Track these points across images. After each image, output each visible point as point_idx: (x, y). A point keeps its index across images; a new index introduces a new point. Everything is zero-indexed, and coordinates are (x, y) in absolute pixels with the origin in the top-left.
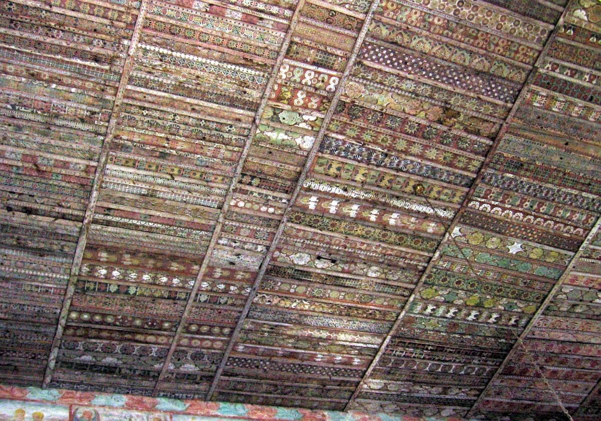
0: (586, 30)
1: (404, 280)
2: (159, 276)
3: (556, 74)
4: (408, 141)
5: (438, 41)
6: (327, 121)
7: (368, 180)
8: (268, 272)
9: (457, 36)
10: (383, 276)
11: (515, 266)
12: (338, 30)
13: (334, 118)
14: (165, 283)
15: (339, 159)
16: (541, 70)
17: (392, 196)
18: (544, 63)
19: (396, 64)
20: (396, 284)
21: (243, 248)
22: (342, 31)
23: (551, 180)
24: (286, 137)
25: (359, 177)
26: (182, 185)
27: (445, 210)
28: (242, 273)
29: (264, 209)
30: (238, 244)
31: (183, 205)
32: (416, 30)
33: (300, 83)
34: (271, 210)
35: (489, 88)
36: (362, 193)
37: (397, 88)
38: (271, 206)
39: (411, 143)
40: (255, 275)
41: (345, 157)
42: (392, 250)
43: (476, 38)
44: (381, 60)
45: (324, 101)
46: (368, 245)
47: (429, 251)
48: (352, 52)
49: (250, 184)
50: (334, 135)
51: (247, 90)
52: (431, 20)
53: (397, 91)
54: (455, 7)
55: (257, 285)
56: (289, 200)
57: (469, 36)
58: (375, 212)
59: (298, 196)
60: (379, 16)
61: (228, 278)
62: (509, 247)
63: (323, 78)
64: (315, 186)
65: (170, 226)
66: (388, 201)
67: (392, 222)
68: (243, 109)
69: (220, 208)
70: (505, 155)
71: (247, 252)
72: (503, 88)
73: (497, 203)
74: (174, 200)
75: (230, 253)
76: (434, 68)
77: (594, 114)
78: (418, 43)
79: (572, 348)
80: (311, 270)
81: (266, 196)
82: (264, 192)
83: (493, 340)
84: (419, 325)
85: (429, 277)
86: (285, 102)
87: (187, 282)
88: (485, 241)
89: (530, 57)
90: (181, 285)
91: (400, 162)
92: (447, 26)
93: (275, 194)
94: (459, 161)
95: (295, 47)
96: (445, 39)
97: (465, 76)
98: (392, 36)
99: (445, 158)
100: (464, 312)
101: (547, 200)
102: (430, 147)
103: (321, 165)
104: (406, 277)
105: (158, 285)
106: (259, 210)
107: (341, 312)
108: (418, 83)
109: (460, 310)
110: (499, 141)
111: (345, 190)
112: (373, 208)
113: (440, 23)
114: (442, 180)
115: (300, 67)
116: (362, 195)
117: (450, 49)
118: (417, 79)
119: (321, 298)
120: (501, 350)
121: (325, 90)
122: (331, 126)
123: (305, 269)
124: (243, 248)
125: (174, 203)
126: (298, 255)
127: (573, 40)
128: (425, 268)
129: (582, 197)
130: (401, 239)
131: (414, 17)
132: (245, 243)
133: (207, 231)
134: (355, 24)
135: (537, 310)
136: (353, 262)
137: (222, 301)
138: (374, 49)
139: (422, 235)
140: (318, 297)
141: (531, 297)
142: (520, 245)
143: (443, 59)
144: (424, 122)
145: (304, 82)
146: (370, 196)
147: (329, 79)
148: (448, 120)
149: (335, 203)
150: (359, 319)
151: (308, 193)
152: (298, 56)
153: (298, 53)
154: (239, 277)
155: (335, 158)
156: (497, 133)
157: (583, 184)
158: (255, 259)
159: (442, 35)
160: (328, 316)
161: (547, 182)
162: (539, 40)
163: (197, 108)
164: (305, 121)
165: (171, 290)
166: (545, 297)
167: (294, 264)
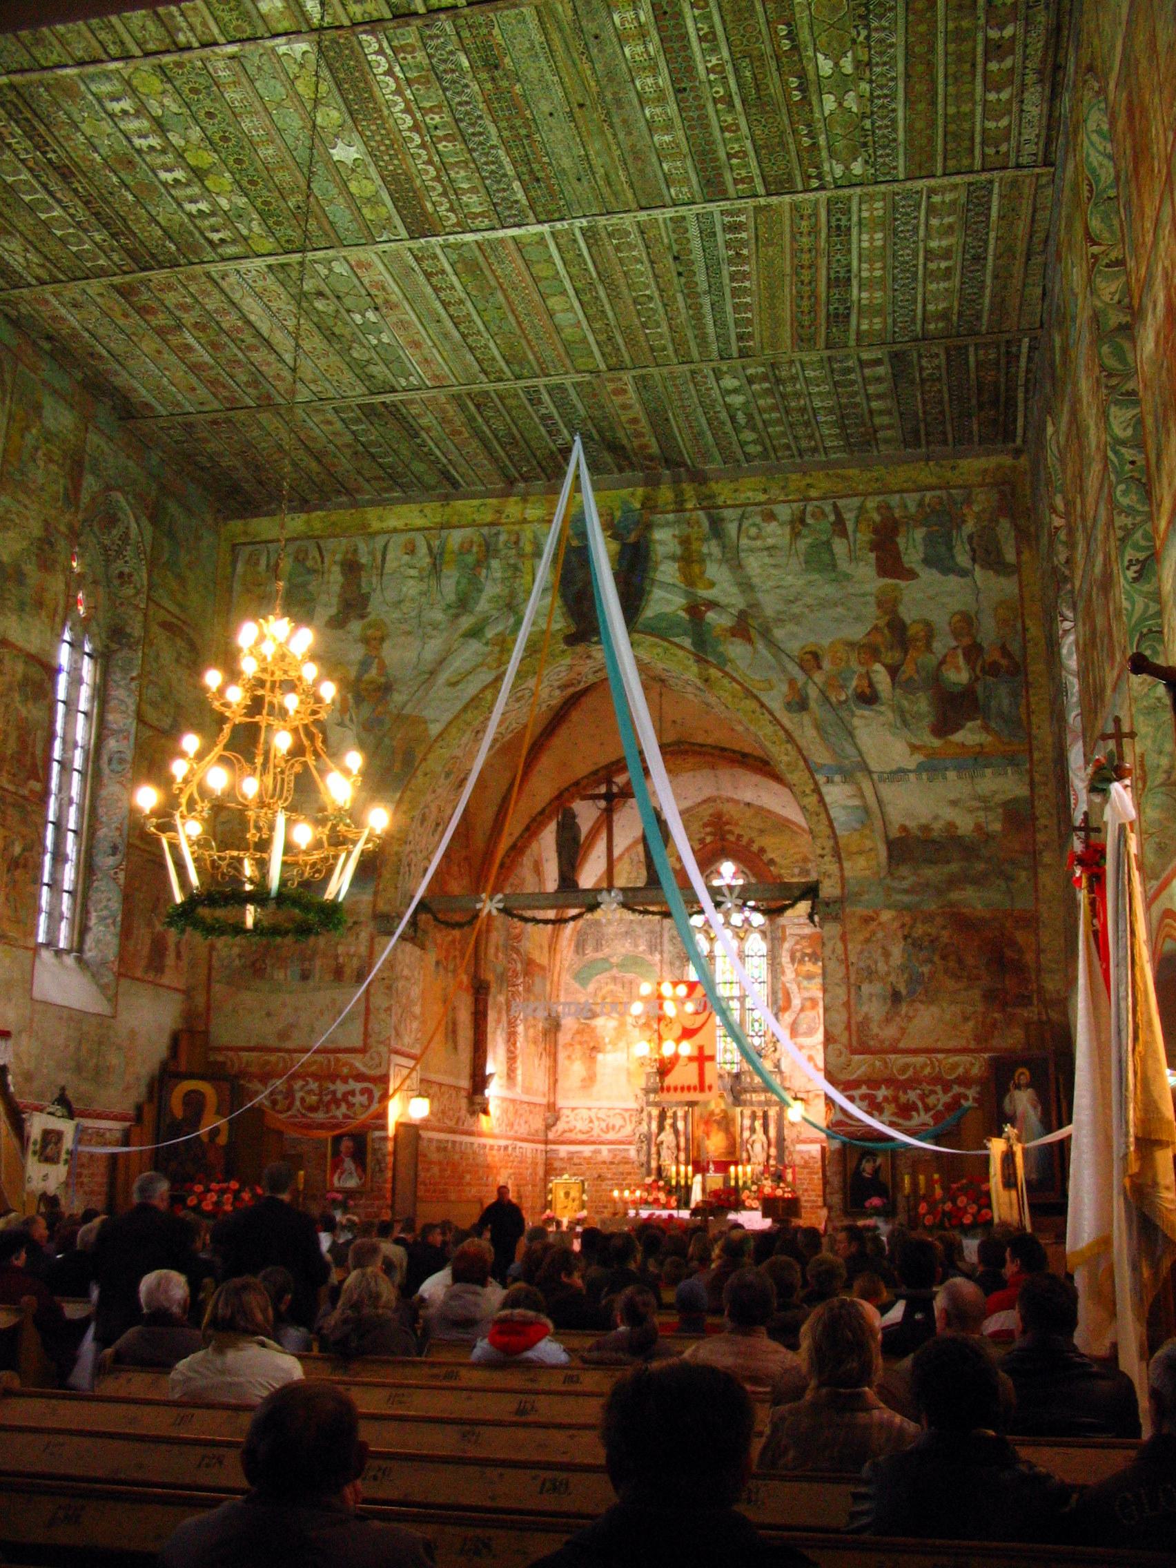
23: (504, 124)
62: (340, 144)
70: (496, 31)
77: (658, 110)
104: (143, 27)
135: (270, 254)
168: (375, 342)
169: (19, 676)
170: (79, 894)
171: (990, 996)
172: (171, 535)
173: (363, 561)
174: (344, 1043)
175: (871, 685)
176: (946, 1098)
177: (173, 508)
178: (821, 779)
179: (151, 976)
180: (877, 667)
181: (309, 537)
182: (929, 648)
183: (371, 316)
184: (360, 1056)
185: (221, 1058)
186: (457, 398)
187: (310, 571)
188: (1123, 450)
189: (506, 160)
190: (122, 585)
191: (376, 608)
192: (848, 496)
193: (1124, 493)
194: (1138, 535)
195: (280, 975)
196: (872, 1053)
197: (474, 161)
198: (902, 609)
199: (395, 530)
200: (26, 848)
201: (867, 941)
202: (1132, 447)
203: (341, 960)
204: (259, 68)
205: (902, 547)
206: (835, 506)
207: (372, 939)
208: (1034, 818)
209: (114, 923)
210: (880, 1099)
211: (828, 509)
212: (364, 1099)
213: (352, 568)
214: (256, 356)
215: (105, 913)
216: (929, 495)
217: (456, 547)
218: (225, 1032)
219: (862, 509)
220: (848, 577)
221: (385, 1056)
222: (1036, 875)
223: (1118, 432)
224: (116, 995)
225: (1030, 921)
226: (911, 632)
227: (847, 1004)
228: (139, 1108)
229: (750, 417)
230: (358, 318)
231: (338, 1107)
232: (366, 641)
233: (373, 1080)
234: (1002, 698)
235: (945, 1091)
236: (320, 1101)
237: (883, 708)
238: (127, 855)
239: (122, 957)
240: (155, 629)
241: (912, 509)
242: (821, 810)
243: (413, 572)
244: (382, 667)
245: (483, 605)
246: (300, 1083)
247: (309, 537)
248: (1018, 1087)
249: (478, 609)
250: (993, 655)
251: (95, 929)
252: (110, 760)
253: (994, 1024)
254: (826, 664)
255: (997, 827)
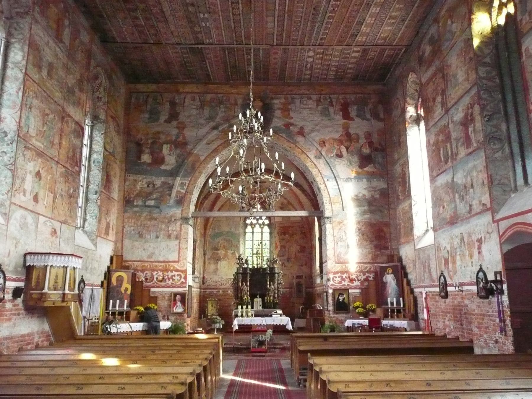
79: (160, 18)
168: (204, 25)
169: (73, 128)
170: (83, 208)
171: (376, 247)
172: (113, 86)
173: (177, 101)
174: (171, 259)
175: (340, 152)
176: (364, 277)
177: (114, 77)
178: (325, 180)
179: (105, 237)
180: (342, 146)
181: (159, 92)
182: (358, 141)
183: (206, 15)
184: (177, 263)
185: (127, 265)
186: (224, 50)
187: (158, 103)
188: (483, 81)
190: (98, 101)
191: (182, 117)
192: (334, 94)
193: (484, 94)
194: (488, 107)
195: (148, 237)
196: (342, 263)
198: (350, 130)
199: (187, 93)
200: (74, 191)
201: (340, 229)
202: (486, 80)
203: (170, 232)
205: (350, 111)
206: (330, 97)
207: (181, 225)
208: (389, 194)
209: (96, 218)
210: (344, 277)
211: (328, 98)
212: (178, 278)
213: (173, 104)
214: (161, 25)
215: (93, 214)
216: (358, 95)
217: (209, 99)
218: (128, 256)
219: (338, 98)
220: (334, 119)
221: (186, 263)
222: (389, 210)
223: (481, 75)
224: (96, 243)
225: (387, 225)
226: (353, 136)
227: (334, 248)
228: (102, 283)
229: (312, 66)
230: (202, 16)
231: (169, 280)
232: (178, 128)
233: (182, 271)
234: (379, 158)
235: (364, 275)
236: (163, 278)
237: (344, 159)
238: (100, 195)
239: (98, 229)
240: (109, 118)
241: (353, 99)
242: (326, 189)
243: (194, 107)
244: (184, 137)
245: (218, 119)
246: (156, 273)
247: (159, 92)
248: (388, 274)
249: (216, 120)
250: (376, 145)
251: (88, 220)
252: (94, 161)
253: (378, 255)
254: (327, 145)
255: (377, 196)
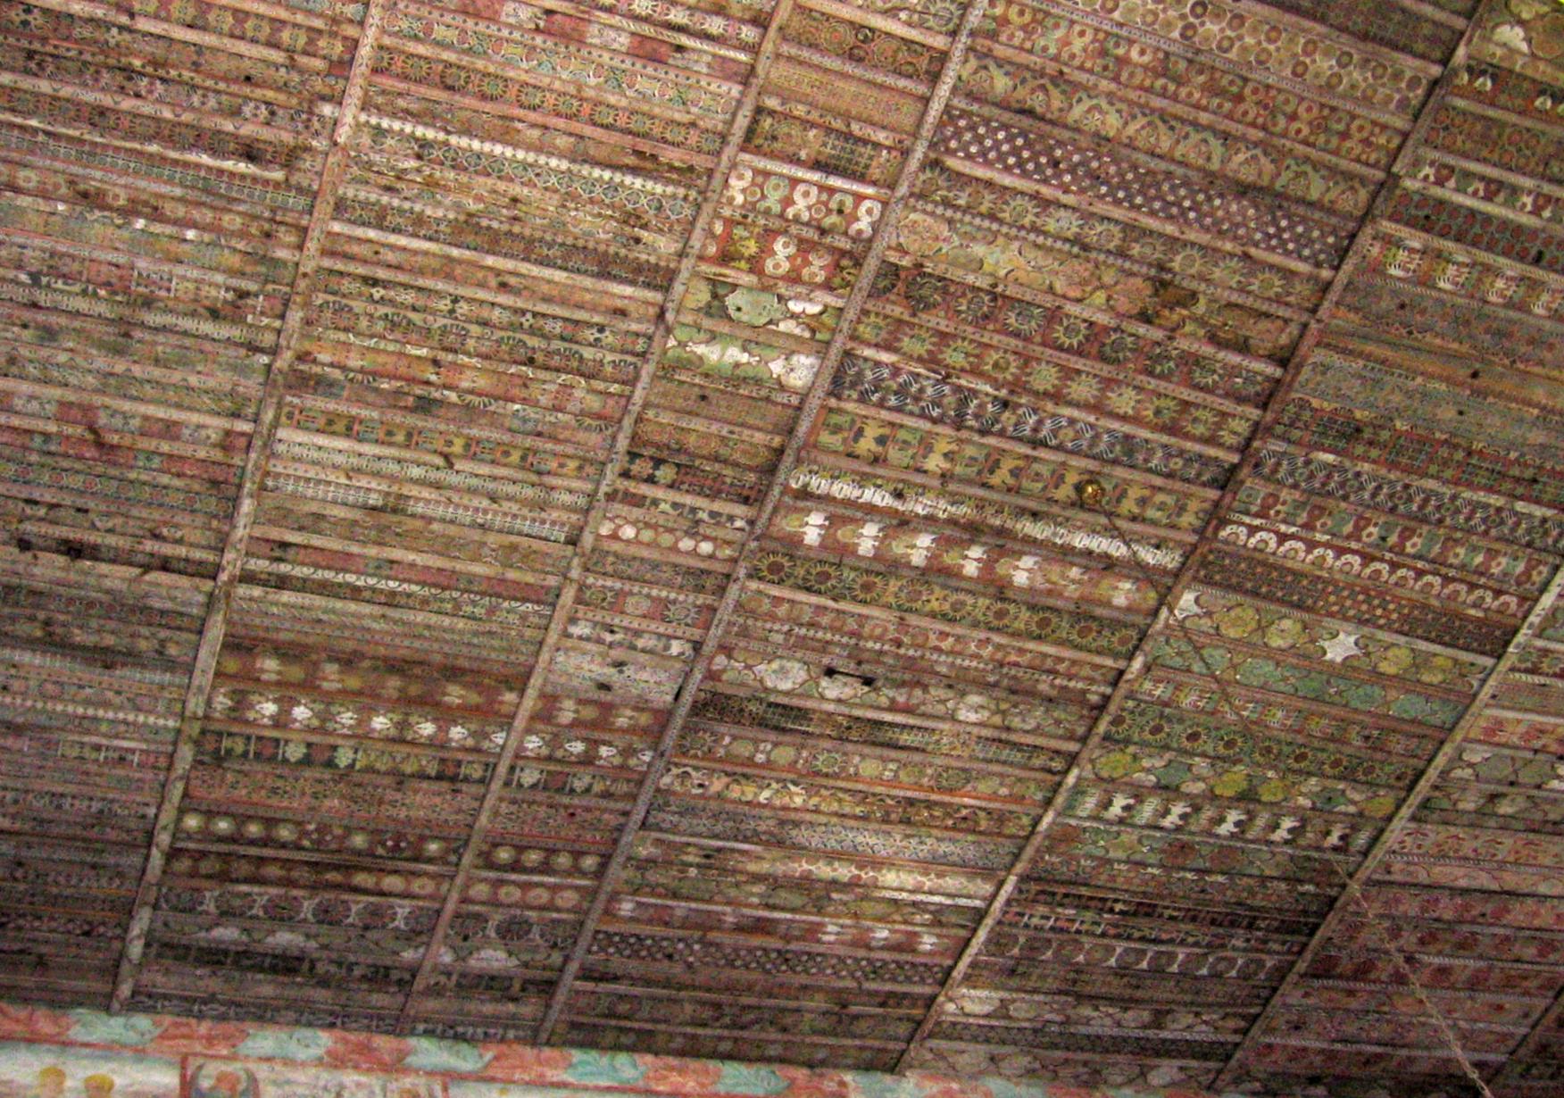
0: (1525, 78)
1: (1052, 729)
2: (413, 719)
3: (1447, 193)
4: (1062, 368)
5: (1141, 106)
6: (851, 314)
7: (959, 470)
8: (698, 709)
9: (1190, 95)
10: (997, 720)
11: (1339, 693)
12: (880, 78)
13: (869, 306)
14: (430, 738)
15: (885, 415)
16: (1408, 183)
17: (1021, 512)
18: (1417, 163)
19: (1030, 166)
20: (1030, 740)
21: (633, 647)
22: (890, 80)
23: (1433, 469)
24: (744, 358)
25: (935, 463)
26: (474, 482)
27: (1158, 547)
28: (629, 713)
29: (686, 544)
30: (618, 637)
31: (476, 535)
32: (1082, 77)
33: (782, 216)
34: (706, 547)
35: (1272, 230)
36: (942, 504)
37: (1034, 229)
38: (706, 538)
39: (1069, 374)
40: (664, 717)
41: (899, 410)
42: (1021, 651)
43: (1239, 98)
44: (992, 155)
45: (845, 262)
46: (958, 638)
47: (1116, 655)
48: (915, 135)
49: (651, 480)
50: (868, 352)
51: (644, 234)
52: (1121, 51)
53: (1032, 237)
54: (1183, 17)
55: (669, 741)
56: (752, 523)
57: (1221, 93)
58: (976, 552)
59: (775, 510)
60: (988, 43)
61: (594, 725)
62: (1326, 644)
63: (841, 203)
64: (819, 484)
65: (444, 589)
66: (1009, 524)
67: (1021, 578)
68: (633, 283)
69: (573, 541)
70: (1315, 403)
71: (643, 658)
72: (1308, 230)
73: (1293, 529)
74: (452, 522)
75: (598, 659)
76: (1130, 176)
77: (1545, 297)
78: (1089, 110)
79: (1489, 908)
80: (809, 704)
81: (694, 510)
82: (688, 500)
83: (1283, 886)
84: (1091, 849)
85: (1117, 721)
86: (743, 265)
87: (486, 736)
88: (1262, 628)
89: (1379, 148)
90: (470, 742)
91: (1040, 422)
92: (1163, 68)
93: (717, 506)
94: (1195, 420)
95: (767, 123)
96: (1157, 102)
97: (1209, 199)
98: (1022, 92)
99: (1158, 412)
100: (1208, 813)
101: (1424, 520)
102: (1118, 382)
103: (837, 429)
104: (1058, 722)
105: (413, 743)
106: (674, 549)
107: (888, 814)
108: (1087, 217)
109: (1197, 809)
110: (1299, 366)
111: (899, 495)
112: (972, 542)
113: (1146, 59)
114: (1150, 470)
115: (781, 176)
116: (943, 509)
117: (1172, 128)
118: (1084, 206)
119: (836, 776)
120: (1305, 912)
121: (846, 233)
122: (861, 328)
123: (795, 702)
124: (633, 647)
125: (452, 530)
126: (775, 665)
127: (1492, 105)
128: (1107, 699)
129: (1516, 513)
130: (1044, 623)
131: (1078, 45)
132: (637, 633)
133: (538, 602)
134: (923, 64)
135: (1398, 808)
136: (918, 684)
137: (578, 785)
138: (973, 128)
139: (1099, 611)
140: (827, 775)
141: (1384, 773)
142: (1352, 639)
143: (1153, 154)
144: (1103, 319)
145: (790, 212)
146: (964, 511)
147: (856, 206)
148: (1166, 312)
149: (871, 529)
150: (935, 832)
151: (801, 504)
152: (777, 145)
153: (774, 138)
154: (622, 722)
155: (872, 412)
156: (1294, 346)
157: (1518, 480)
158: (663, 676)
159: (1149, 90)
160: (852, 823)
161: (1424, 475)
162: (1403, 104)
163: (512, 281)
164: (794, 316)
165: (446, 755)
166: (1420, 774)
167: (766, 689)
189: (1481, 496)
197: (1455, 529)
204: (1180, 654)
